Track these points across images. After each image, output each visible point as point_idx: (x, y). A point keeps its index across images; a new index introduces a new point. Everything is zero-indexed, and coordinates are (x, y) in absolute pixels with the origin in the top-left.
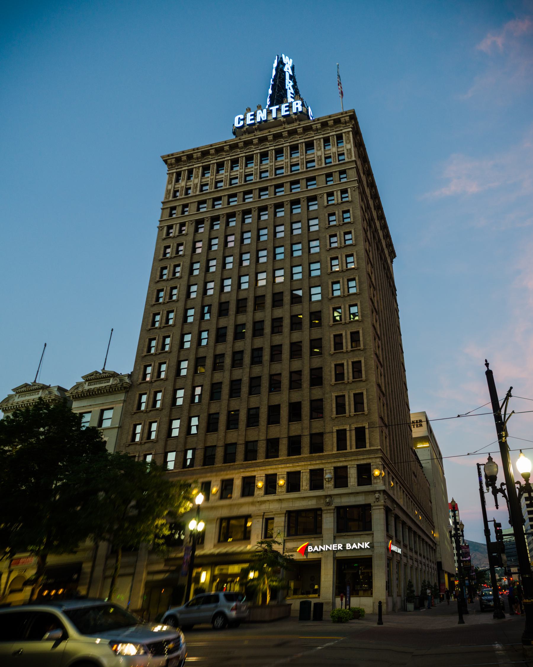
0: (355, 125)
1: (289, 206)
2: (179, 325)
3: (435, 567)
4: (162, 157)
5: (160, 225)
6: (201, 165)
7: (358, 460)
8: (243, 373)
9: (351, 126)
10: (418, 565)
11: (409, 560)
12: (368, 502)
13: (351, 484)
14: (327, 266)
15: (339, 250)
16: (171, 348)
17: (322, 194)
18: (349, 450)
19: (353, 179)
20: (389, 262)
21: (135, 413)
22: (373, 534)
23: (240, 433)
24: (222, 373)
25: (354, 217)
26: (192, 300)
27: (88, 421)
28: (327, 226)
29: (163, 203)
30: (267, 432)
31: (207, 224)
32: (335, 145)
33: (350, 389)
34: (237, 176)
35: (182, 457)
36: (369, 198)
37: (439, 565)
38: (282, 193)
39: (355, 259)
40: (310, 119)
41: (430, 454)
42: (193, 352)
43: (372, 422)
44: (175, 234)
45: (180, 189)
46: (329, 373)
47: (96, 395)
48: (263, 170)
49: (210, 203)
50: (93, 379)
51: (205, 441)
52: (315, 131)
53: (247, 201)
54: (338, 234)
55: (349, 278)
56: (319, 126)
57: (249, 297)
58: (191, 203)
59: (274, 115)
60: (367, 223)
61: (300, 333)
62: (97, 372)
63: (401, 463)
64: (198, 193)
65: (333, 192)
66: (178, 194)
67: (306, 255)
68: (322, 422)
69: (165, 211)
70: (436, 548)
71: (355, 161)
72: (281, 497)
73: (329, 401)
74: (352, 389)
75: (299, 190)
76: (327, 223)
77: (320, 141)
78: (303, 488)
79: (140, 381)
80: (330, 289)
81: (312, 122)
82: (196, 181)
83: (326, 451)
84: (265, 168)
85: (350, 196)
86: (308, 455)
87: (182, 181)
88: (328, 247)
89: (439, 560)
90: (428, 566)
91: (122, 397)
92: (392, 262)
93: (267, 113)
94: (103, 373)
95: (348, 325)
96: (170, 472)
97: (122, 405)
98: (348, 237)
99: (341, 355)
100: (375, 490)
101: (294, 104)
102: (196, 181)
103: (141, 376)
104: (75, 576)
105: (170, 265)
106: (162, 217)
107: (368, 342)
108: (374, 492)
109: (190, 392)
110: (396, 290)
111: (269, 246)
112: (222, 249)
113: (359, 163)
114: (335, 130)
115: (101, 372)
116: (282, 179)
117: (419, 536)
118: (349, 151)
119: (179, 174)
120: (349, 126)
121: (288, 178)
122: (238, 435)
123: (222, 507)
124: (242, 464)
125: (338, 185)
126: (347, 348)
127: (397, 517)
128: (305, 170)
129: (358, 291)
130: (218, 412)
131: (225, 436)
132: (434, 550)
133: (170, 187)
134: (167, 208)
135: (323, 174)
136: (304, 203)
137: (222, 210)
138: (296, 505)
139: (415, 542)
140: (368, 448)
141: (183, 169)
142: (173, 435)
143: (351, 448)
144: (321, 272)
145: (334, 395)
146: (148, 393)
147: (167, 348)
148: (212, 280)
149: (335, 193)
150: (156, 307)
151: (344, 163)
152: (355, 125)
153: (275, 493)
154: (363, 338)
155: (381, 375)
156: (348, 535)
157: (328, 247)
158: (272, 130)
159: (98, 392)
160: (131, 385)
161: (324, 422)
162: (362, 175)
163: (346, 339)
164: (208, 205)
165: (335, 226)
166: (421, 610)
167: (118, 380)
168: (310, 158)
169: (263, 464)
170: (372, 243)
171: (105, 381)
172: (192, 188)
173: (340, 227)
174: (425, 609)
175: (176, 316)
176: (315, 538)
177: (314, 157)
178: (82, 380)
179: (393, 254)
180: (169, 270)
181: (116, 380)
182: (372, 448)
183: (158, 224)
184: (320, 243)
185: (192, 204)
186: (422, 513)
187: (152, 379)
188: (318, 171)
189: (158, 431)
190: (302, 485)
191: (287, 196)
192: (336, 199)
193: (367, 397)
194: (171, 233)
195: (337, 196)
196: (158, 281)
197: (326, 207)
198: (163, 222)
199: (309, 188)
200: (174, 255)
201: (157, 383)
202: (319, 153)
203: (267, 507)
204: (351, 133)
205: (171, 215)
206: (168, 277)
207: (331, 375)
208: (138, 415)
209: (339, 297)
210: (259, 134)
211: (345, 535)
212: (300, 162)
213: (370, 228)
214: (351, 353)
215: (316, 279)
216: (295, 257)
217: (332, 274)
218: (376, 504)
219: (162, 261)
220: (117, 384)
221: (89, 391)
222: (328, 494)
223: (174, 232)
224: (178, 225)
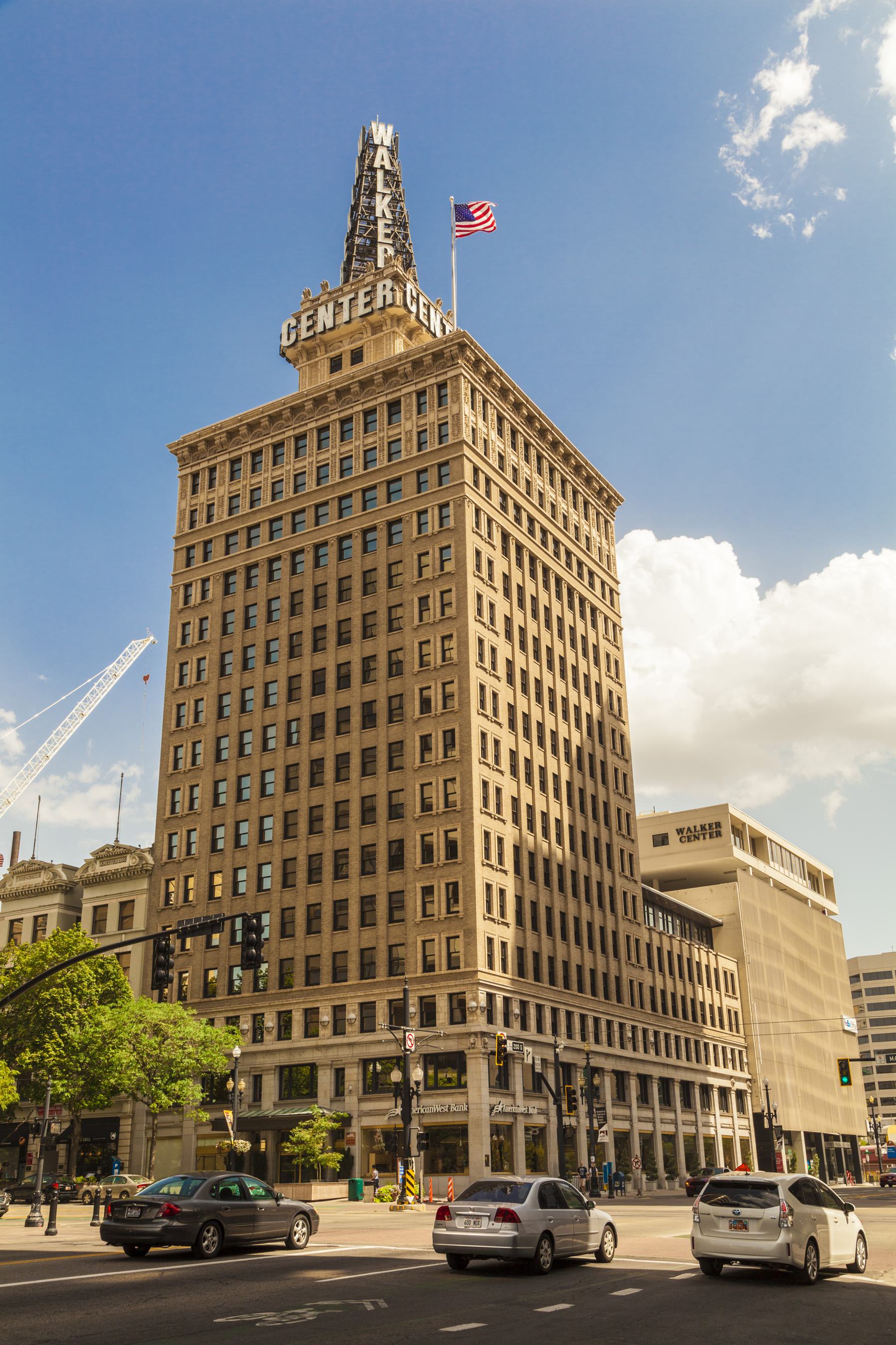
7: (449, 986)
8: (298, 848)
18: (437, 972)
21: (163, 910)
29: (176, 538)
35: (227, 978)
61: (374, 780)
62: (108, 846)
77: (411, 398)
83: (408, 973)
91: (144, 884)
97: (145, 896)
99: (430, 820)
103: (165, 852)
104: (114, 1136)
106: (175, 570)
108: (469, 1034)
119: (195, 476)
122: (295, 946)
123: (280, 1051)
124: (302, 991)
133: (455, 410)
134: (182, 548)
138: (372, 1051)
140: (462, 970)
141: (220, 459)
145: (419, 885)
146: (176, 879)
149: (430, 510)
150: (176, 736)
169: (328, 990)
178: (91, 857)
182: (468, 969)
193: (464, 889)
203: (335, 1053)
207: (415, 854)
208: (166, 912)
218: (471, 1051)
221: (102, 875)
224: (199, 582)
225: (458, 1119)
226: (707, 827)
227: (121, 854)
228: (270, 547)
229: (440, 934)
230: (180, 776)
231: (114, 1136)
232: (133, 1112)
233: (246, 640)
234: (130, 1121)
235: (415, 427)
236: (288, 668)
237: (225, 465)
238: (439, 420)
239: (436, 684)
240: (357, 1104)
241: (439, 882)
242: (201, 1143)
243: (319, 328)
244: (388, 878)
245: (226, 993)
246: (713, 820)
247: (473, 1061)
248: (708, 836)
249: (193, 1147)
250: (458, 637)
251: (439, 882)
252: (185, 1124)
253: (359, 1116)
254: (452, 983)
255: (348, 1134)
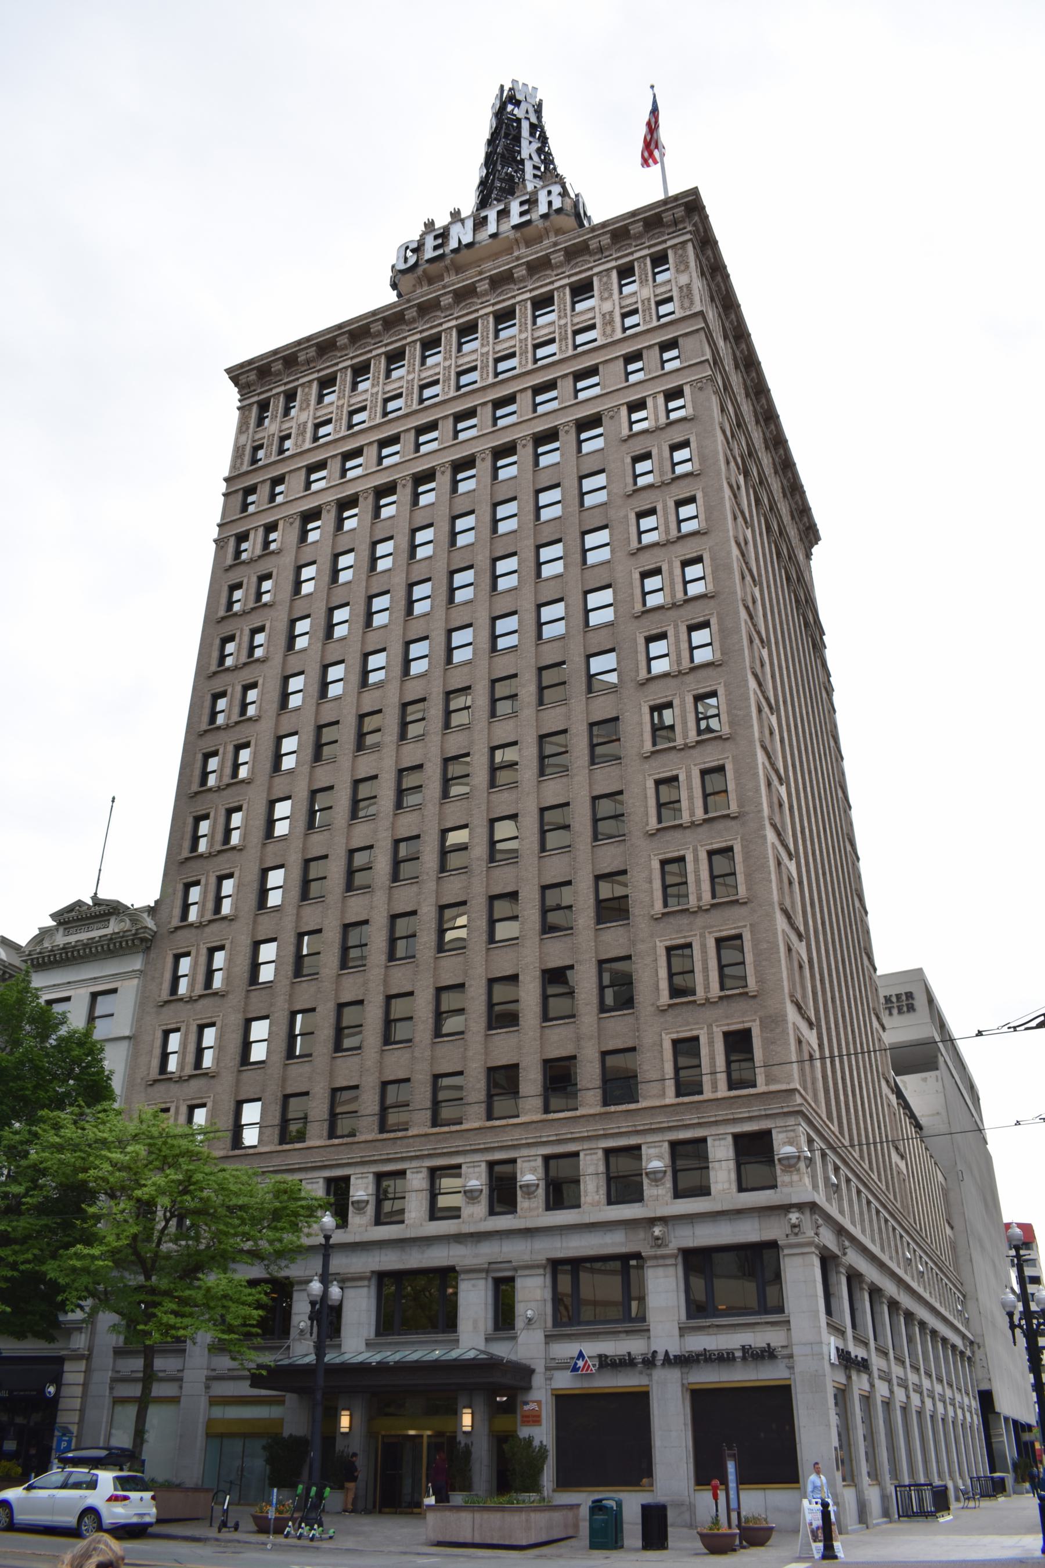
0: (700, 225)
1: (530, 449)
2: (262, 778)
3: (975, 1404)
4: (228, 371)
5: (219, 534)
6: (315, 376)
8: (419, 894)
9: (689, 228)
10: (923, 1402)
11: (896, 1388)
12: (767, 1236)
13: (720, 1187)
14: (633, 594)
15: (664, 549)
16: (244, 837)
17: (616, 410)
18: (708, 1094)
19: (698, 360)
20: (801, 557)
22: (789, 1322)
23: (416, 1054)
24: (368, 896)
25: (703, 459)
26: (293, 714)
27: (76, 1019)
28: (630, 488)
29: (226, 480)
30: (486, 1048)
31: (329, 518)
32: (647, 280)
33: (705, 927)
34: (399, 391)
36: (741, 398)
37: (986, 1399)
38: (513, 419)
39: (708, 571)
40: (584, 226)
41: (941, 1089)
42: (297, 844)
43: (770, 1017)
44: (253, 552)
45: (265, 441)
46: (647, 886)
47: (82, 957)
48: (465, 367)
49: (335, 466)
50: (74, 920)
51: (332, 1074)
52: (596, 253)
53: (424, 449)
54: (659, 508)
55: (693, 622)
56: (606, 240)
57: (430, 694)
58: (290, 472)
59: (492, 227)
60: (738, 468)
62: (79, 903)
63: (863, 1053)
64: (308, 445)
65: (644, 398)
66: (261, 454)
67: (576, 570)
68: (630, 1020)
69: (232, 498)
70: (973, 1352)
71: (701, 314)
72: (530, 1224)
73: (648, 960)
74: (712, 927)
75: (554, 405)
76: (630, 480)
77: (609, 277)
78: (589, 1199)
79: (176, 922)
80: (642, 658)
81: (589, 233)
82: (303, 417)
83: (645, 1098)
84: (469, 362)
85: (689, 405)
86: (599, 1109)
87: (271, 422)
88: (635, 544)
89: (984, 1387)
90: (954, 1405)
91: (136, 963)
92: (808, 556)
93: (475, 225)
94: (95, 904)
95: (692, 751)
96: (251, 1151)
98: (686, 511)
100: (787, 1202)
101: (543, 197)
102: (303, 417)
103: (177, 912)
105: (242, 631)
107: (750, 794)
108: (786, 1208)
109: (291, 949)
110: (822, 633)
111: (480, 557)
112: (364, 577)
113: (711, 315)
114: (647, 244)
115: (90, 903)
116: (511, 383)
117: (922, 1324)
118: (685, 289)
120: (685, 228)
121: (528, 377)
125: (656, 380)
126: (692, 814)
127: (854, 1278)
128: (570, 352)
129: (718, 656)
130: (360, 998)
131: (381, 1063)
132: (969, 1358)
133: (243, 439)
135: (617, 358)
136: (568, 438)
137: (364, 479)
139: (910, 1339)
140: (761, 1088)
142: (254, 1058)
143: (715, 1088)
144: (615, 612)
146: (193, 953)
147: (235, 838)
148: (340, 659)
149: (650, 402)
151: (671, 323)
152: (700, 225)
153: (516, 1212)
154: (737, 785)
155: (790, 883)
156: (718, 1326)
157: (635, 544)
158: (487, 266)
159: (84, 949)
160: (155, 933)
161: (637, 1019)
162: (721, 343)
163: (690, 788)
164: (330, 473)
165: (651, 486)
166: (941, 1520)
167: (128, 921)
168: (582, 322)
170: (751, 516)
171: (100, 925)
172: (293, 436)
173: (664, 488)
174: (950, 1517)
175: (255, 755)
176: (627, 1332)
177: (594, 318)
179: (810, 534)
180: (240, 644)
181: (122, 921)
182: (773, 1088)
183: (215, 533)
184: (611, 535)
185: (292, 475)
186: (925, 1257)
187: (202, 916)
188: (603, 352)
189: (220, 1047)
190: (585, 1191)
191: (523, 426)
192: (652, 417)
194: (245, 550)
195: (656, 407)
196: (215, 673)
197: (625, 441)
198: (228, 527)
199: (582, 396)
200: (251, 604)
201: (214, 927)
202: (607, 306)
204: (690, 247)
205: (245, 506)
206: (237, 660)
209: (665, 675)
210: (454, 281)
211: (709, 1326)
212: (557, 335)
213: (745, 477)
214: (706, 827)
215: (604, 631)
216: (547, 579)
217: (646, 616)
218: (793, 1240)
219: (222, 624)
220: (125, 932)
221: (65, 948)
222: (658, 1215)
223: (251, 548)
225: (787, 1382)
226: (894, 999)
227: (101, 915)
228: (378, 474)
229: (710, 1026)
230: (210, 796)
231: (52, 1389)
232: (90, 1349)
233: (334, 598)
234: (82, 1365)
235: (617, 308)
236: (405, 629)
237: (310, 387)
238: (655, 296)
239: (676, 627)
240: (542, 1346)
241: (702, 936)
242: (218, 1412)
243: (453, 244)
244: (596, 937)
245: (276, 1141)
246: (902, 990)
247: (798, 1261)
248: (895, 1011)
249: (202, 1419)
250: (712, 559)
251: (702, 936)
252: (187, 1375)
253: (547, 1369)
254: (743, 1112)
255: (526, 1403)
